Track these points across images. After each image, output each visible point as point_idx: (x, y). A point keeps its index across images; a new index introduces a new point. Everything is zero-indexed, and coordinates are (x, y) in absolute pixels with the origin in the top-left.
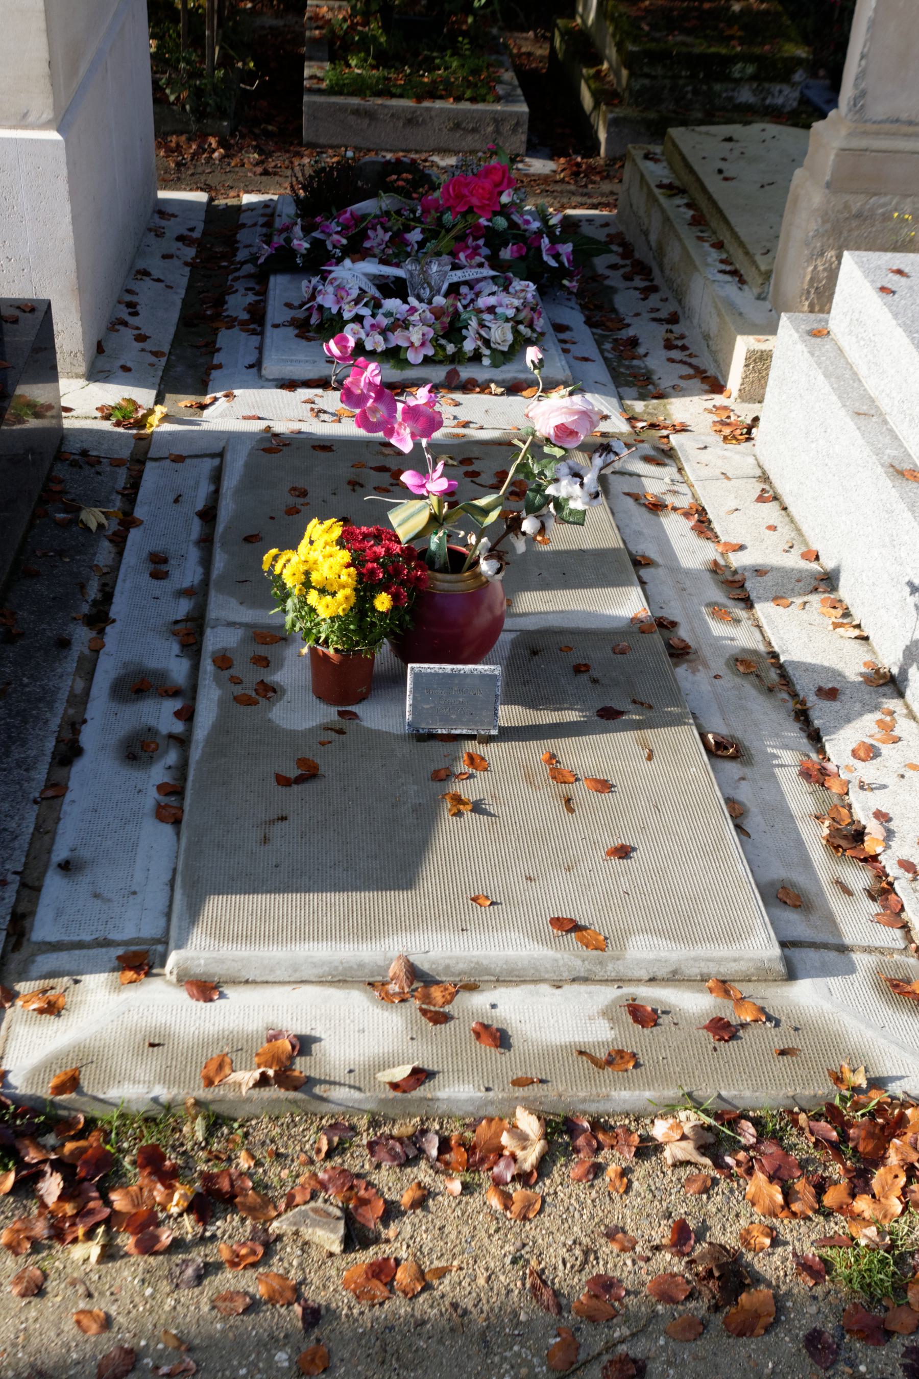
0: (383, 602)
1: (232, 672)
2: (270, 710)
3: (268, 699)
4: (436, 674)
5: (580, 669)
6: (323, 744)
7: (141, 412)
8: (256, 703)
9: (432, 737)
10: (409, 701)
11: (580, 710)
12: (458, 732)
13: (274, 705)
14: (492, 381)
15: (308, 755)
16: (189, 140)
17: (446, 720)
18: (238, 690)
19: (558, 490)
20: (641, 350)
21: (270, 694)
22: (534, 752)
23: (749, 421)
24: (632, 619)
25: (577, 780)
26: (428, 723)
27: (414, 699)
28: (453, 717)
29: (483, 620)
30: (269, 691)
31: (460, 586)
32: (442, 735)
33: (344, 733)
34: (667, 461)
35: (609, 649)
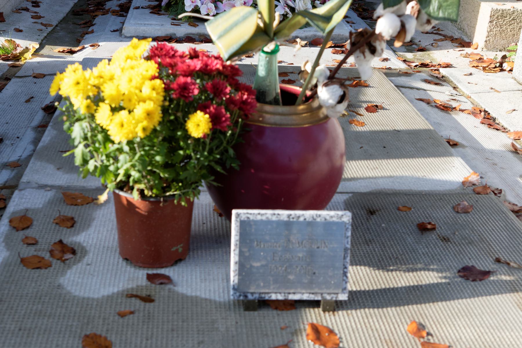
0: (198, 124)
1: (29, 232)
2: (63, 273)
3: (64, 261)
4: (268, 222)
5: (423, 228)
6: (122, 315)
7: (19, 50)
8: (48, 266)
9: (264, 304)
10: (234, 257)
11: (437, 271)
12: (297, 297)
13: (69, 267)
14: (297, 37)
15: (100, 330)
17: (283, 283)
18: (29, 252)
21: (68, 256)
22: (396, 321)
23: (499, 59)
24: (463, 183)
26: (258, 286)
27: (241, 254)
29: (319, 167)
30: (66, 252)
32: (277, 301)
34: (443, 83)
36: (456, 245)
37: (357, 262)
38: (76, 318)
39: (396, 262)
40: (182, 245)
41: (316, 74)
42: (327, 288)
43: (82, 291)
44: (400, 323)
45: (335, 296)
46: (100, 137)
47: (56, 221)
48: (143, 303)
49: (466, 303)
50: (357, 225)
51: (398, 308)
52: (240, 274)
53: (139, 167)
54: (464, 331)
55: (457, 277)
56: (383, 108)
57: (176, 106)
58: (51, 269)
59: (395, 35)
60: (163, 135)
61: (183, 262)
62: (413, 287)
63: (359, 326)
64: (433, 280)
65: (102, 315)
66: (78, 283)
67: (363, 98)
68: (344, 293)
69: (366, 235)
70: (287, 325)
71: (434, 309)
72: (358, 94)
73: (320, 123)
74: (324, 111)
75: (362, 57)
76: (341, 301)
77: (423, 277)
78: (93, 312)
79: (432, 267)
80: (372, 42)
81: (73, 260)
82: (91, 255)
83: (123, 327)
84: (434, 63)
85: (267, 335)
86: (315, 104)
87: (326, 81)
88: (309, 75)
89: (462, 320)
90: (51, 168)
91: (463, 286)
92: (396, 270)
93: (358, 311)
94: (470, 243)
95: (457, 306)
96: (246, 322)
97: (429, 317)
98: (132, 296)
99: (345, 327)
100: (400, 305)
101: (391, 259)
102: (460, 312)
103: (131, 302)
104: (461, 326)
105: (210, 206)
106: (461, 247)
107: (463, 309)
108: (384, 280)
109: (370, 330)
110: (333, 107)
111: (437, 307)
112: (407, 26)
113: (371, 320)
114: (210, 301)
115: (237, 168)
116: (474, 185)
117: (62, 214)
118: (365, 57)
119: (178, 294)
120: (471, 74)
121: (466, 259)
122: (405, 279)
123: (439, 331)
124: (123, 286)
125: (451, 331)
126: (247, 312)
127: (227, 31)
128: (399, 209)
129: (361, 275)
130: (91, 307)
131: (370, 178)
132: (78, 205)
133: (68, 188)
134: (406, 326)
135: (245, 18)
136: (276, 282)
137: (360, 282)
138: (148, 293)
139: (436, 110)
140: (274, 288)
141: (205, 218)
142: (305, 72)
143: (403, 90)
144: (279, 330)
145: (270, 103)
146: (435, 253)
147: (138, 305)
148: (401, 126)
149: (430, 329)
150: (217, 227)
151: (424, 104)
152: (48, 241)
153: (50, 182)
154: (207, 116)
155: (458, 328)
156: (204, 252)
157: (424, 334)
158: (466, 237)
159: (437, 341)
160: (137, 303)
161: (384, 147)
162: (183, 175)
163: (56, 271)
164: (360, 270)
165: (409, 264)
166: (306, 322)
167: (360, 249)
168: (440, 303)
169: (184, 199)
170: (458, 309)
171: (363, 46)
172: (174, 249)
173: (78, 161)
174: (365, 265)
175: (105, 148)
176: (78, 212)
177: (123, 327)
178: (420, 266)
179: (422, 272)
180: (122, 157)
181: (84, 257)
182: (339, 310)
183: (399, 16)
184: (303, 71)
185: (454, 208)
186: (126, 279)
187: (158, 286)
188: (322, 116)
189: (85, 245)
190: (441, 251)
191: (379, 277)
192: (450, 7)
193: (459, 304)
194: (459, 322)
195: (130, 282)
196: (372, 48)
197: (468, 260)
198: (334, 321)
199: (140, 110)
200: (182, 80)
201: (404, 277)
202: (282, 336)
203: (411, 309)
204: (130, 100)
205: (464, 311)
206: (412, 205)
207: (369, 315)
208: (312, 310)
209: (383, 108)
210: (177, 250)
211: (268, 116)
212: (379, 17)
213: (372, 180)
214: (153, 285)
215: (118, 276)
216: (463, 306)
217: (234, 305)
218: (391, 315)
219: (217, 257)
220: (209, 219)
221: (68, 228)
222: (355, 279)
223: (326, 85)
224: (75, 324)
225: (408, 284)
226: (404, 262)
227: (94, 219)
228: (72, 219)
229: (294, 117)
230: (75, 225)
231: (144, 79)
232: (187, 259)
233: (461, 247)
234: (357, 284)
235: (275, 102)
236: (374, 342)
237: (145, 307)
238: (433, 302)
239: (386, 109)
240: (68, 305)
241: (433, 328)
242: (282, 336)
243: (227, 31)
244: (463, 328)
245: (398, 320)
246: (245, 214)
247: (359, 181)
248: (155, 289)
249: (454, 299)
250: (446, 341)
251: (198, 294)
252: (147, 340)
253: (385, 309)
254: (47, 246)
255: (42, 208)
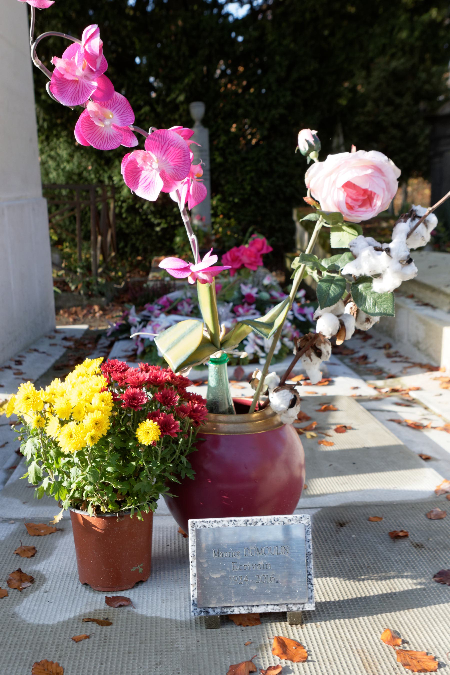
0: (148, 432)
2: (20, 601)
3: (21, 590)
5: (395, 537)
6: (77, 640)
9: (227, 619)
11: (412, 577)
13: (26, 596)
15: (52, 656)
16: (83, 309)
17: (244, 595)
19: (358, 267)
20: (371, 360)
21: (26, 584)
22: (369, 630)
24: (436, 492)
25: (440, 665)
27: (199, 565)
28: (253, 588)
29: (278, 475)
30: (23, 581)
31: (249, 427)
33: (110, 624)
34: (414, 405)
35: (422, 516)
36: (431, 551)
37: (327, 573)
38: (28, 646)
39: (368, 571)
40: (142, 565)
41: (265, 382)
42: (292, 598)
43: (38, 618)
44: (373, 632)
45: (301, 606)
46: (52, 452)
47: (17, 552)
48: (100, 627)
49: (444, 608)
50: (326, 537)
51: (370, 617)
52: (199, 588)
53: (91, 479)
54: (443, 637)
55: (433, 582)
56: (351, 428)
57: (126, 414)
58: (7, 599)
59: (335, 333)
60: (113, 445)
61: (144, 584)
62: (386, 594)
63: (329, 638)
64: (407, 586)
65: (56, 641)
66: (33, 610)
67: (331, 421)
68: (311, 603)
69: (336, 547)
70: (252, 640)
71: (409, 616)
72: (327, 417)
73: (275, 430)
74: (279, 419)
75: (309, 360)
76: (309, 611)
77: (396, 585)
78: (46, 639)
79: (406, 574)
80: (316, 345)
81: (30, 588)
82: (50, 582)
83: (77, 653)
84: (404, 388)
85: (230, 652)
86: (269, 412)
87: (276, 387)
88: (260, 383)
89: (440, 625)
90: (17, 503)
91: (440, 591)
92: (368, 579)
93: (328, 622)
94: (445, 548)
95: (434, 612)
96: (207, 640)
97: (404, 625)
98: (89, 620)
99: (313, 639)
100: (372, 614)
101: (362, 569)
102: (437, 617)
103: (87, 627)
104: (439, 631)
105: (175, 528)
106: (436, 552)
107: (440, 614)
108: (356, 589)
109: (340, 641)
110: (285, 412)
111: (412, 613)
112: (346, 324)
113: (341, 631)
114: (171, 620)
115: (193, 478)
116: (447, 492)
117: (23, 545)
118: (311, 360)
119: (137, 615)
120: (441, 395)
121: (441, 564)
122: (378, 588)
123: (415, 639)
124: (81, 611)
125: (428, 638)
126: (209, 630)
127: (174, 344)
128: (369, 520)
129: (331, 586)
130: (46, 634)
131: (339, 493)
132: (41, 536)
133: (32, 520)
134: (379, 635)
135: (191, 330)
136: (237, 594)
137: (330, 593)
138: (106, 617)
139: (408, 429)
140: (236, 601)
141: (169, 540)
142: (255, 380)
143: (374, 413)
144: (243, 645)
145: (224, 413)
146: (408, 560)
147: (94, 629)
148: (371, 443)
149: (406, 636)
150: (181, 548)
151: (395, 425)
152: (8, 571)
153: (14, 516)
154: (156, 423)
155: (436, 634)
156: (166, 573)
157: (399, 642)
158: (440, 543)
159: (413, 649)
160: (94, 626)
161: (354, 463)
162: (137, 487)
163: (12, 600)
164: (329, 582)
165: (382, 572)
166: (271, 637)
167: (329, 560)
168: (415, 610)
169: (139, 513)
170: (436, 615)
171: (308, 349)
172: (134, 569)
173: (32, 480)
174: (335, 576)
175: (57, 463)
176: (40, 543)
177: (77, 653)
178: (392, 573)
179: (396, 580)
180: (73, 471)
181: (42, 585)
182: (308, 623)
183: (338, 316)
184: (254, 379)
185: (426, 515)
186: (84, 604)
187: (117, 609)
188: (276, 423)
189: (44, 573)
190: (415, 558)
191: (350, 587)
192: (385, 303)
193: (437, 609)
194: (437, 628)
195: (88, 607)
196: (318, 351)
197: (444, 564)
198: (301, 634)
199: (88, 421)
200: (131, 391)
201: (376, 585)
202: (246, 652)
203: (385, 617)
204: (80, 413)
205: (442, 617)
206: (383, 515)
207: (339, 626)
208: (278, 624)
209: (351, 428)
210: (138, 570)
211: (221, 425)
212: (318, 318)
213: (342, 495)
214: (112, 608)
215: (75, 602)
216: (441, 611)
217: (196, 623)
218: (363, 624)
219: (180, 576)
220: (173, 541)
221: (28, 557)
222: (324, 591)
223: (276, 391)
224: (26, 652)
225: (381, 593)
226: (376, 570)
227: (56, 548)
228: (34, 548)
229: (248, 425)
230: (36, 555)
231: (93, 391)
232: (149, 581)
233: (436, 552)
234: (326, 595)
235: (230, 412)
236: (345, 652)
237: (101, 631)
238: (408, 609)
239: (355, 429)
240: (20, 633)
241: (408, 636)
242: (246, 652)
243: (174, 344)
244: (441, 634)
245: (371, 629)
246: (201, 522)
247: (329, 496)
248: (115, 613)
249: (430, 605)
250: (424, 647)
251: (159, 614)
252: (102, 664)
253: (356, 619)
254: (5, 577)
255: (4, 540)
